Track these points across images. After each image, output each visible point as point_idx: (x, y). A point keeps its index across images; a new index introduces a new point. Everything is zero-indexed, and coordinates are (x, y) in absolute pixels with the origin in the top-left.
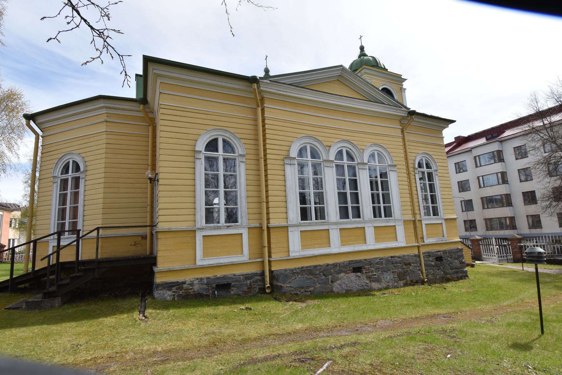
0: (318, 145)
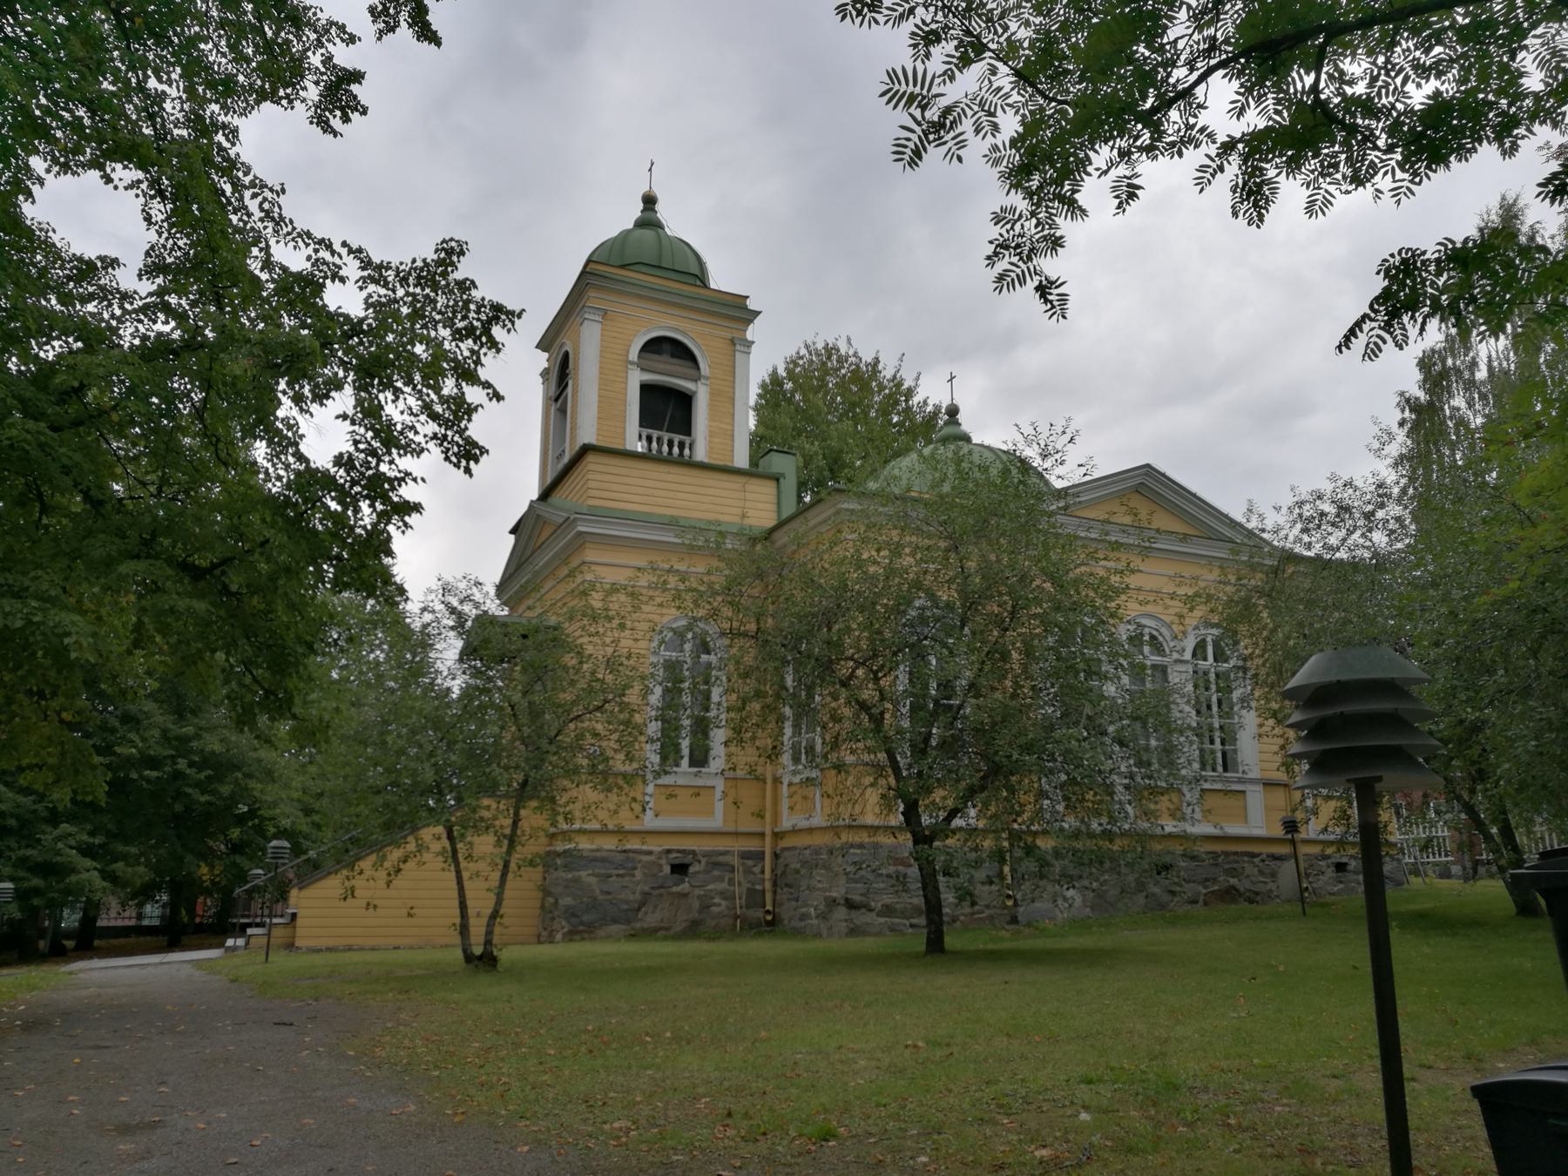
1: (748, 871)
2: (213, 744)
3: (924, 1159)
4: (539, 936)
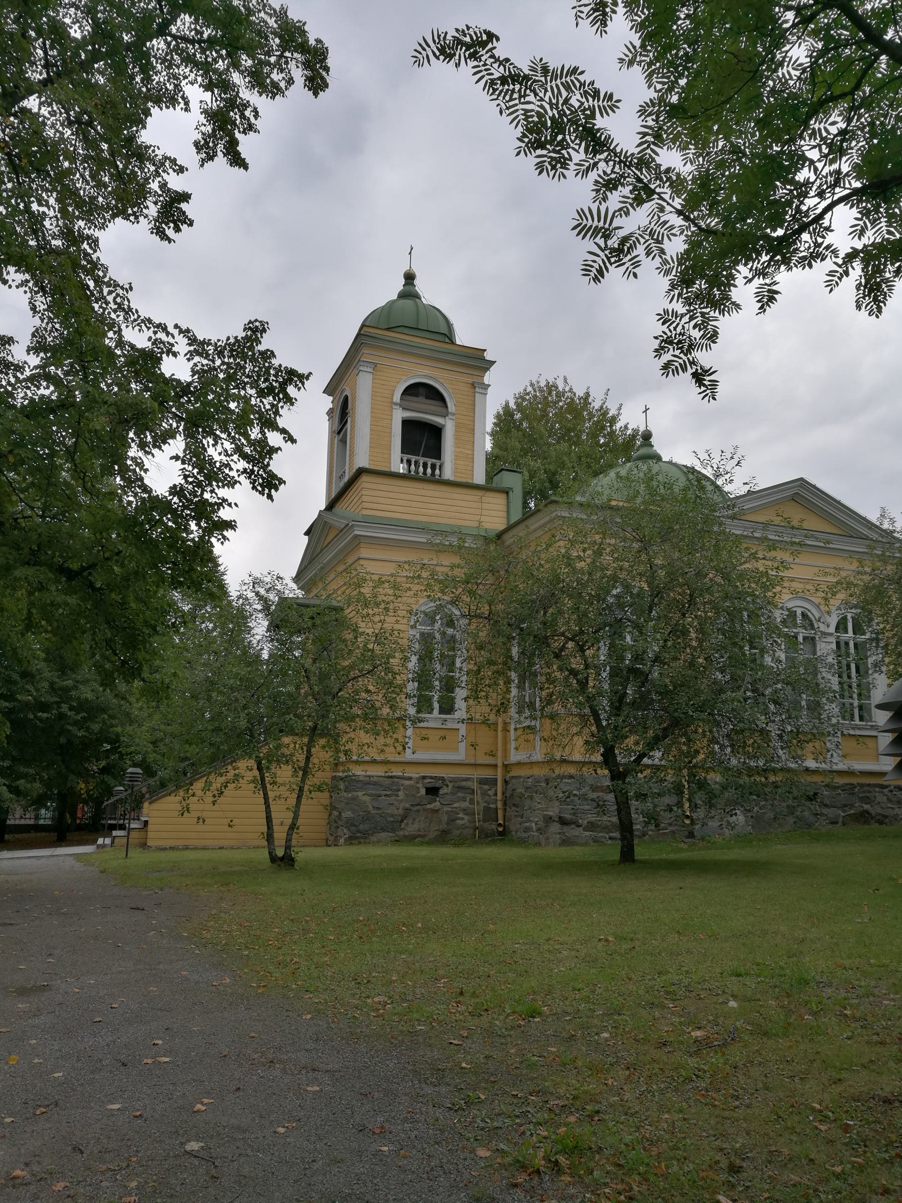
1: (485, 794)
2: (86, 693)
3: (606, 1035)
4: (327, 840)
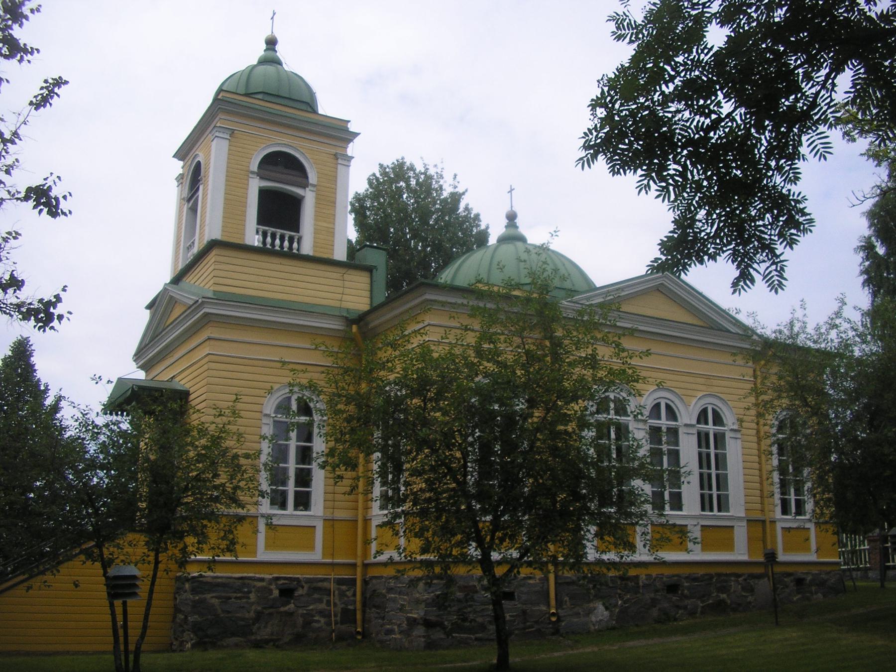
0: (677, 401)
1: (342, 594)
4: (172, 644)
